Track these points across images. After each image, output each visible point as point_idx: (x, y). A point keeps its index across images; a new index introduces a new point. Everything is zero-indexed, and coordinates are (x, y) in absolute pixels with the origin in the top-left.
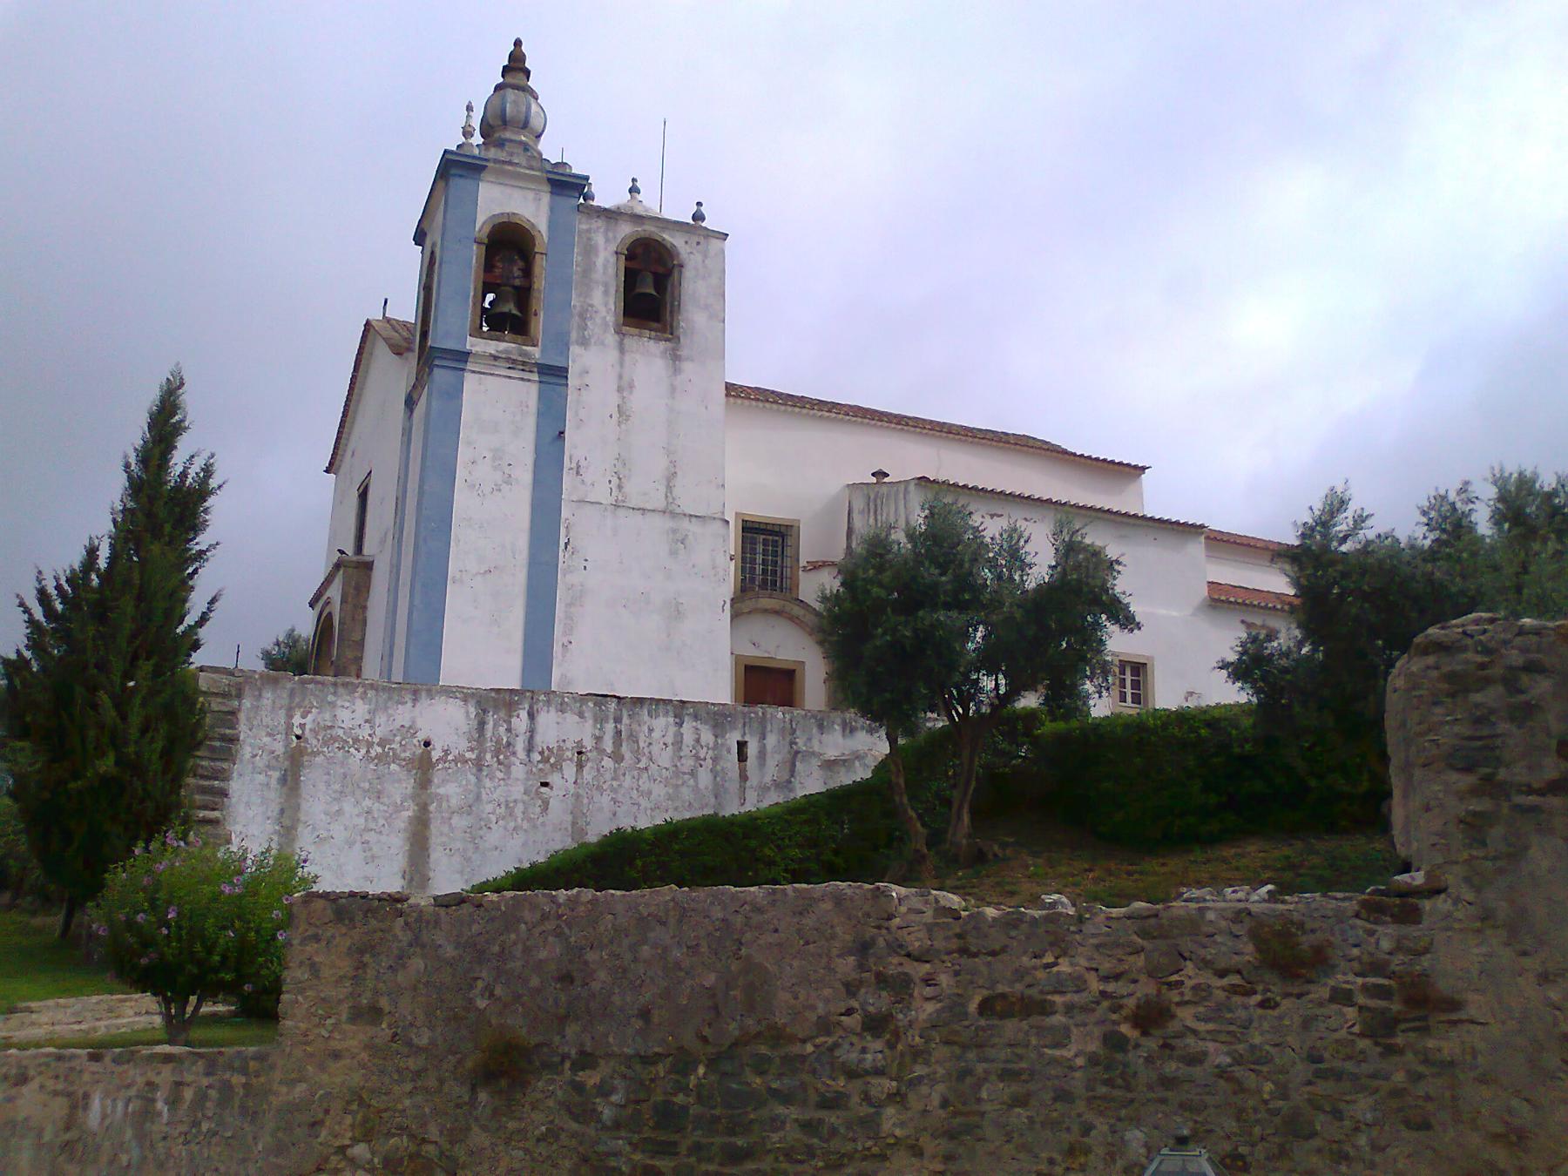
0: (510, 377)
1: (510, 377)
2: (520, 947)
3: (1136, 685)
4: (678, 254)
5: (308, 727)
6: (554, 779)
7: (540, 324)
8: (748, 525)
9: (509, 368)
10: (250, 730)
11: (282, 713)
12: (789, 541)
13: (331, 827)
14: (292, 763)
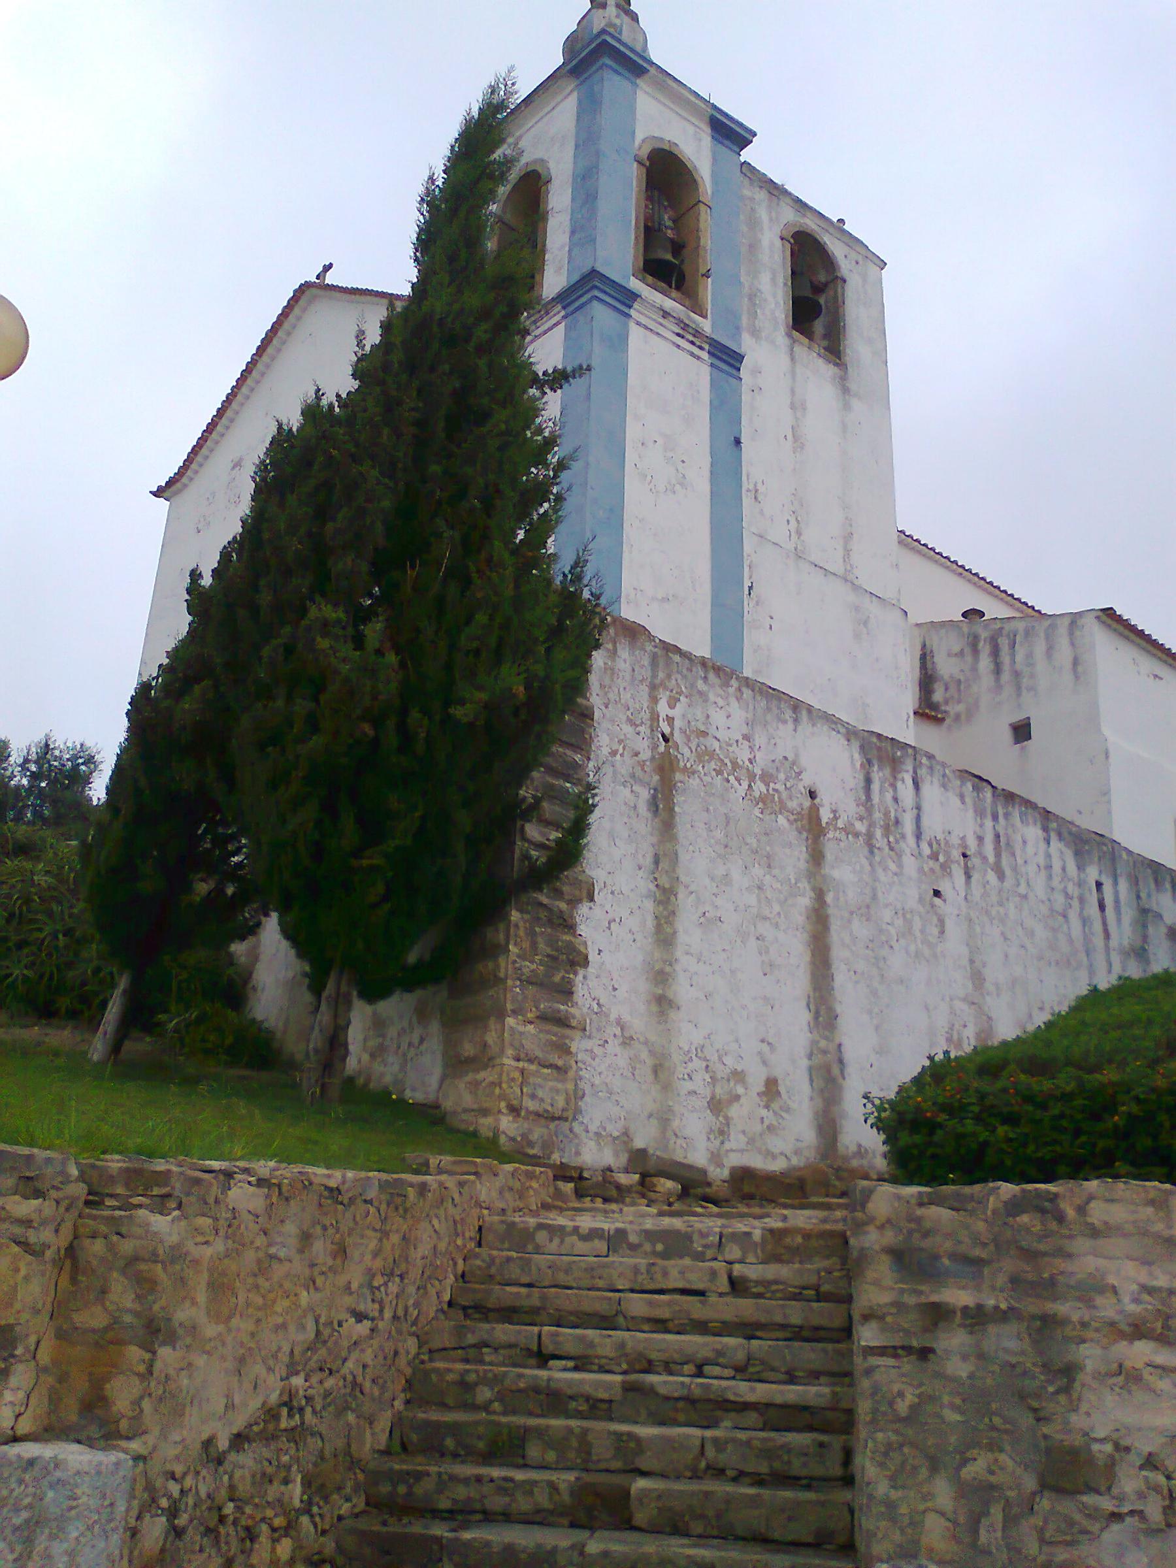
0: (678, 346)
1: (678, 346)
5: (678, 723)
6: (944, 887)
10: (606, 707)
11: (644, 690)
13: (718, 901)
14: (662, 779)
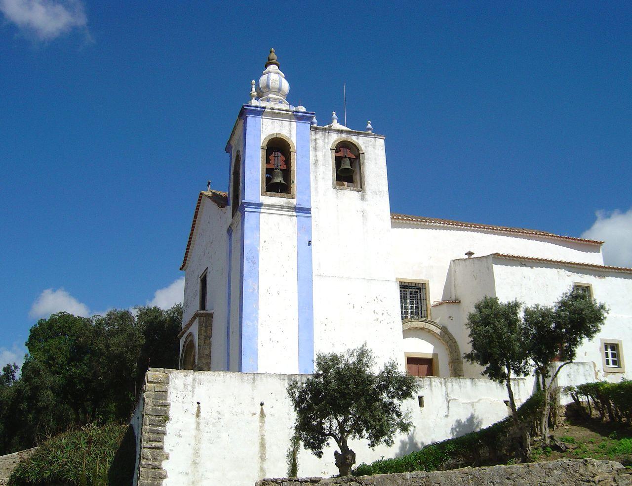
3: (613, 355)
7: (296, 187)
8: (403, 284)
12: (423, 291)
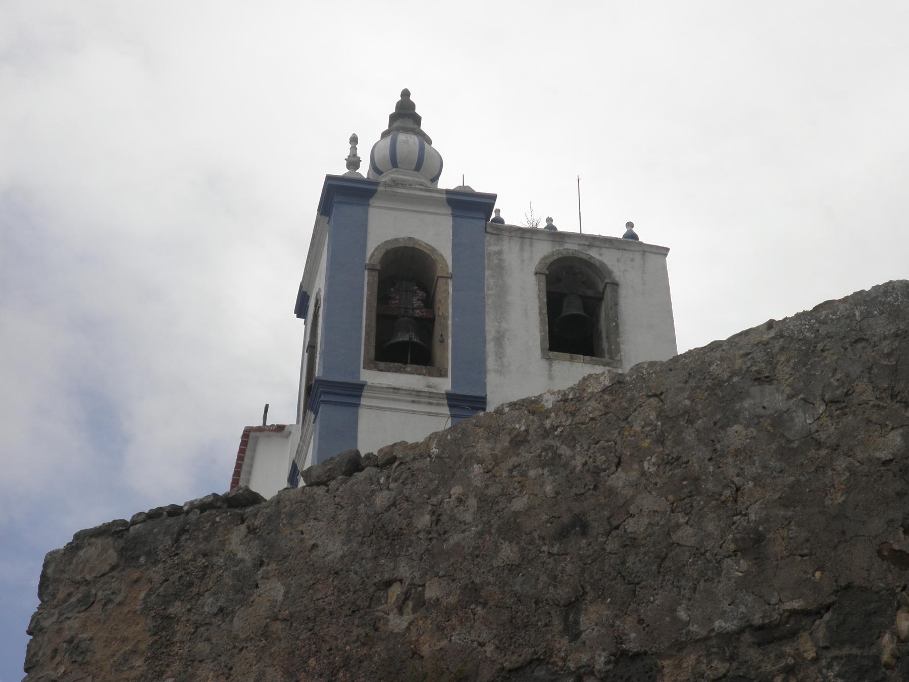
2: (473, 502)
4: (610, 273)
9: (413, 402)
